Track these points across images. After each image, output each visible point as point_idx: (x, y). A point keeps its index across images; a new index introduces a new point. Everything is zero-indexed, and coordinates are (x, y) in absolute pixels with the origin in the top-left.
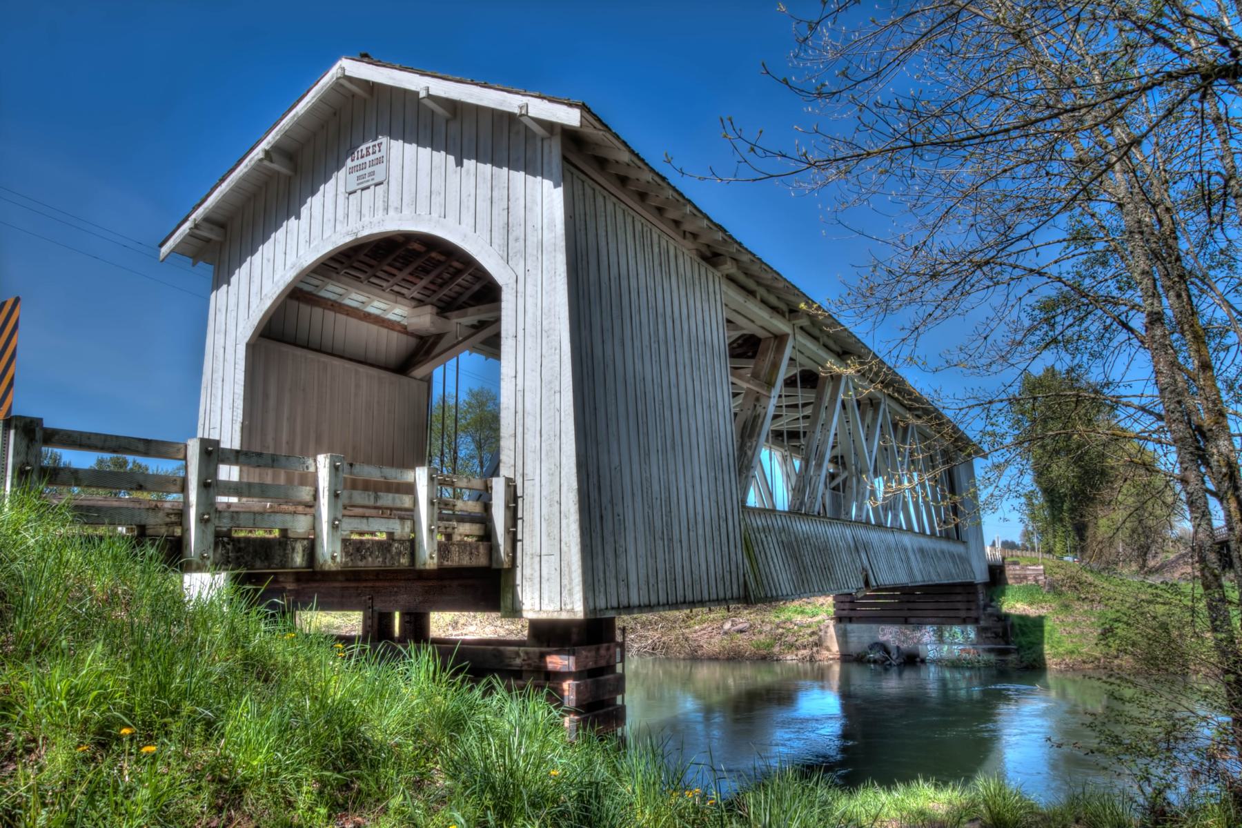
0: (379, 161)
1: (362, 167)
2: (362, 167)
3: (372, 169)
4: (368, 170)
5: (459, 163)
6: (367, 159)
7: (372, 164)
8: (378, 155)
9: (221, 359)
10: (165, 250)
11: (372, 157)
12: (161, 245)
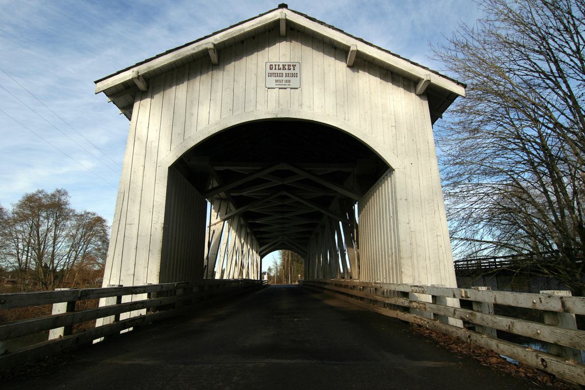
0: (294, 75)
1: (281, 75)
2: (281, 75)
3: (287, 78)
6: (284, 72)
7: (287, 75)
8: (292, 71)
9: (141, 174)
11: (287, 71)
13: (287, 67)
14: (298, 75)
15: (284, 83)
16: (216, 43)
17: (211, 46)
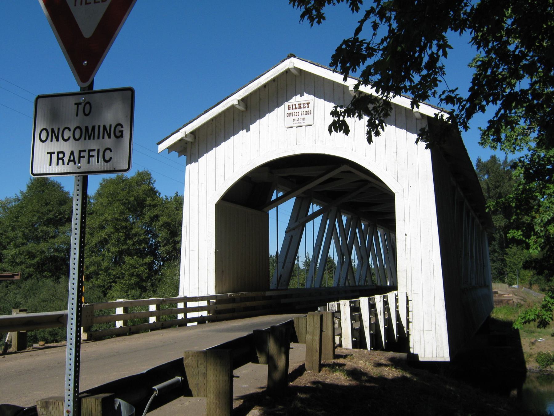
0: (309, 113)
2: (297, 114)
3: (303, 117)
4: (300, 117)
8: (307, 109)
10: (163, 147)
11: (302, 110)
12: (159, 144)
14: (312, 112)
16: (240, 98)
17: (236, 103)
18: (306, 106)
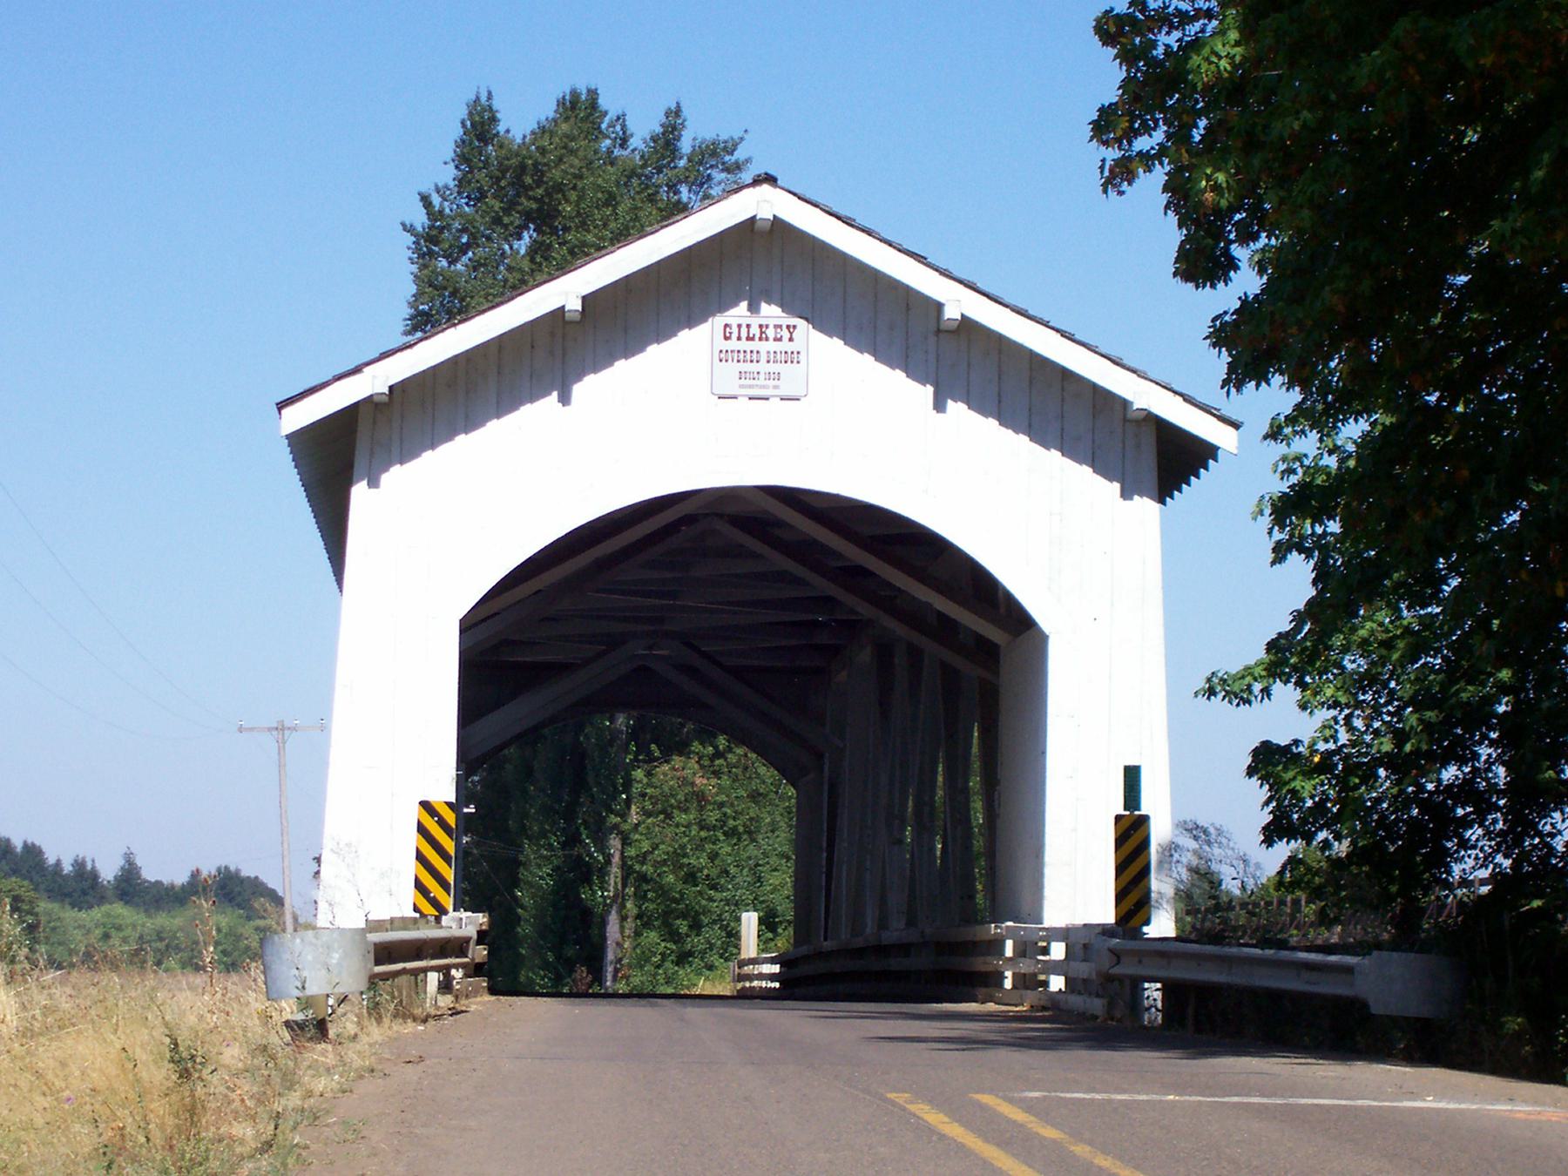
0: (791, 358)
2: (754, 356)
3: (773, 367)
4: (763, 367)
5: (939, 406)
6: (764, 347)
8: (785, 345)
11: (771, 346)
13: (771, 332)
14: (802, 357)
15: (761, 382)
18: (786, 334)
